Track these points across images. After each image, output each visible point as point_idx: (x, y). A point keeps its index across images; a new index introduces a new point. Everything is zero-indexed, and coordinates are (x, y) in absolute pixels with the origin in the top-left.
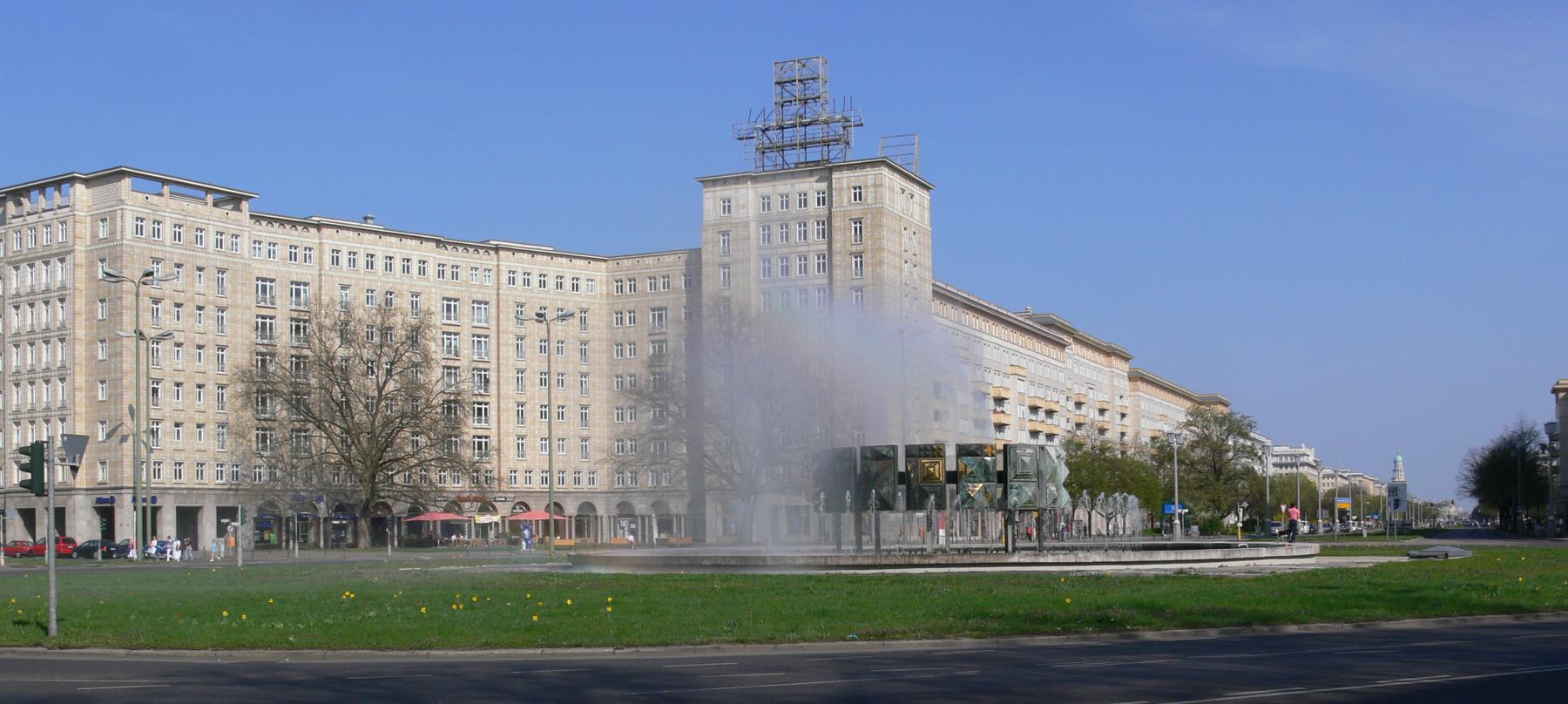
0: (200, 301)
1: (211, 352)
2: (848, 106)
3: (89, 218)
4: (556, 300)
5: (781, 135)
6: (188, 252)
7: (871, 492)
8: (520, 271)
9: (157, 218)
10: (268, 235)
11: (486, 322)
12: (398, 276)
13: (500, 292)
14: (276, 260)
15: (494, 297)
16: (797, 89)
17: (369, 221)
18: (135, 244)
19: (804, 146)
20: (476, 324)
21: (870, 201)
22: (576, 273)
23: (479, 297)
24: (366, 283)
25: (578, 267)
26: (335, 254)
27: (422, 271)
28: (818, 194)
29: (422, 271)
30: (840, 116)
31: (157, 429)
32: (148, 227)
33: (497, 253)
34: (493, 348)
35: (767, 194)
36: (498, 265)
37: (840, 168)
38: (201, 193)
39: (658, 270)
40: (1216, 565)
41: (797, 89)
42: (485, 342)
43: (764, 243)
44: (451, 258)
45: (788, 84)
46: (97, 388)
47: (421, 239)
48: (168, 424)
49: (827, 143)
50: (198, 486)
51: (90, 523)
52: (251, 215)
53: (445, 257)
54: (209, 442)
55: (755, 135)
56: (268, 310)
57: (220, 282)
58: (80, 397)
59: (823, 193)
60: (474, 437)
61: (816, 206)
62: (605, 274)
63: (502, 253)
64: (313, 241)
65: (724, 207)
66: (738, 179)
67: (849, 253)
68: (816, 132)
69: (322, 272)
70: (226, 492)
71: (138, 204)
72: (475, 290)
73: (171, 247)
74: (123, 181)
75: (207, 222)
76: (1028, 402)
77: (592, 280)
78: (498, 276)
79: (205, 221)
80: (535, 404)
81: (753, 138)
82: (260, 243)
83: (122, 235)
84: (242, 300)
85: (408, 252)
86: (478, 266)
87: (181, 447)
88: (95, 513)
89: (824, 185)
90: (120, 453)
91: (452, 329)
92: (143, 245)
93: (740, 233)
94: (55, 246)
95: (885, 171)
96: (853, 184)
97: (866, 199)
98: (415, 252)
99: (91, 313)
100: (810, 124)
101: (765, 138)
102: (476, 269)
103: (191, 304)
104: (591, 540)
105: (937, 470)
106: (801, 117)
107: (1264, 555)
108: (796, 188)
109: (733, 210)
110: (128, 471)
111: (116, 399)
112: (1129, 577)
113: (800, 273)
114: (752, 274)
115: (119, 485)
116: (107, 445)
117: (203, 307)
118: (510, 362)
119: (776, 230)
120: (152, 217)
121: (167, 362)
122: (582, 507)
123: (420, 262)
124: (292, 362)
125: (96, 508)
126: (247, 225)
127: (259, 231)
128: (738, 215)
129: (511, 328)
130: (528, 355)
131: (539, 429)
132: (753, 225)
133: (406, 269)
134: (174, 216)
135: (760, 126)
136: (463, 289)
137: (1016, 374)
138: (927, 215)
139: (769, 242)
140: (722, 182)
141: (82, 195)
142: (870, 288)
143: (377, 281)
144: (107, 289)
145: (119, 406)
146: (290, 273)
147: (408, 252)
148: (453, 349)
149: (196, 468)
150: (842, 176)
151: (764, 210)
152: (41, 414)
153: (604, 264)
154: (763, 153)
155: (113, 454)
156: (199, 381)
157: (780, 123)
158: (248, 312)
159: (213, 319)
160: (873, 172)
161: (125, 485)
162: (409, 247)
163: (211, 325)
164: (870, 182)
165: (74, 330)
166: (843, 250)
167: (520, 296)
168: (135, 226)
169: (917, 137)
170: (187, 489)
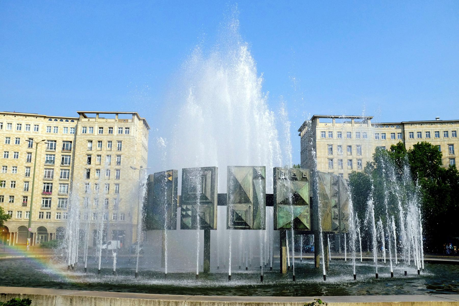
92: (324, 141)
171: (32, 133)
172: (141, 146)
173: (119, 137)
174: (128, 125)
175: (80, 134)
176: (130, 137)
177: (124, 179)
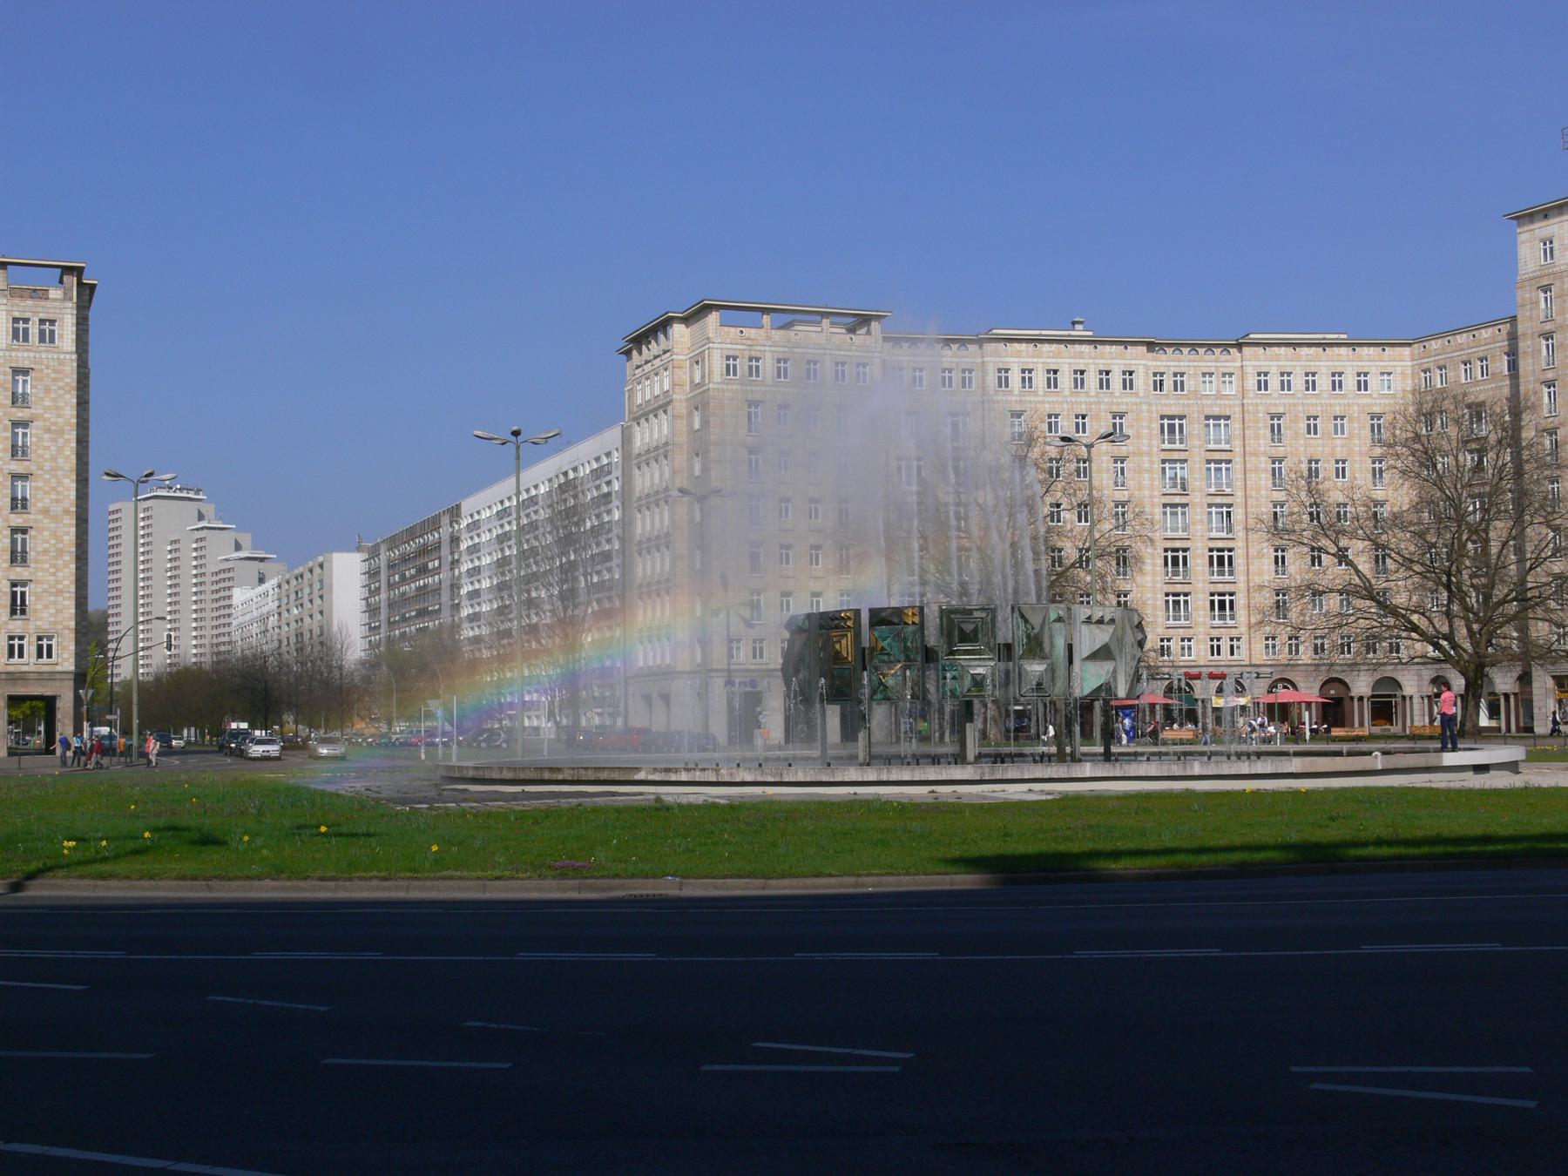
4: (1331, 405)
7: (860, 679)
9: (754, 354)
11: (1228, 442)
12: (1093, 393)
15: (1238, 409)
20: (1212, 446)
22: (1364, 366)
23: (1216, 411)
24: (1047, 406)
25: (1365, 358)
26: (1003, 374)
27: (1128, 385)
29: (1128, 385)
33: (1240, 351)
34: (1239, 476)
38: (819, 318)
39: (1474, 350)
40: (924, 790)
42: (1227, 469)
44: (1173, 363)
47: (1125, 344)
52: (884, 337)
53: (1164, 363)
60: (1167, 595)
62: (1410, 363)
64: (973, 360)
65: (1545, 250)
71: (729, 341)
72: (1209, 402)
75: (822, 352)
77: (1389, 374)
78: (1243, 380)
85: (1105, 361)
86: (1213, 370)
91: (1175, 456)
98: (1115, 361)
102: (1211, 374)
104: (1395, 729)
105: (844, 645)
107: (1088, 775)
109: (1556, 253)
112: (832, 803)
118: (1263, 492)
122: (1379, 683)
133: (1104, 384)
134: (777, 349)
136: (1191, 402)
140: (1556, 211)
141: (682, 336)
143: (1062, 402)
147: (1105, 361)
148: (1179, 481)
167: (1275, 405)
168: (724, 366)
171: (1275, 399)
172: (67, 384)
173: (19, 355)
174: (51, 311)
175: (719, 380)
176: (62, 356)
177: (46, 512)
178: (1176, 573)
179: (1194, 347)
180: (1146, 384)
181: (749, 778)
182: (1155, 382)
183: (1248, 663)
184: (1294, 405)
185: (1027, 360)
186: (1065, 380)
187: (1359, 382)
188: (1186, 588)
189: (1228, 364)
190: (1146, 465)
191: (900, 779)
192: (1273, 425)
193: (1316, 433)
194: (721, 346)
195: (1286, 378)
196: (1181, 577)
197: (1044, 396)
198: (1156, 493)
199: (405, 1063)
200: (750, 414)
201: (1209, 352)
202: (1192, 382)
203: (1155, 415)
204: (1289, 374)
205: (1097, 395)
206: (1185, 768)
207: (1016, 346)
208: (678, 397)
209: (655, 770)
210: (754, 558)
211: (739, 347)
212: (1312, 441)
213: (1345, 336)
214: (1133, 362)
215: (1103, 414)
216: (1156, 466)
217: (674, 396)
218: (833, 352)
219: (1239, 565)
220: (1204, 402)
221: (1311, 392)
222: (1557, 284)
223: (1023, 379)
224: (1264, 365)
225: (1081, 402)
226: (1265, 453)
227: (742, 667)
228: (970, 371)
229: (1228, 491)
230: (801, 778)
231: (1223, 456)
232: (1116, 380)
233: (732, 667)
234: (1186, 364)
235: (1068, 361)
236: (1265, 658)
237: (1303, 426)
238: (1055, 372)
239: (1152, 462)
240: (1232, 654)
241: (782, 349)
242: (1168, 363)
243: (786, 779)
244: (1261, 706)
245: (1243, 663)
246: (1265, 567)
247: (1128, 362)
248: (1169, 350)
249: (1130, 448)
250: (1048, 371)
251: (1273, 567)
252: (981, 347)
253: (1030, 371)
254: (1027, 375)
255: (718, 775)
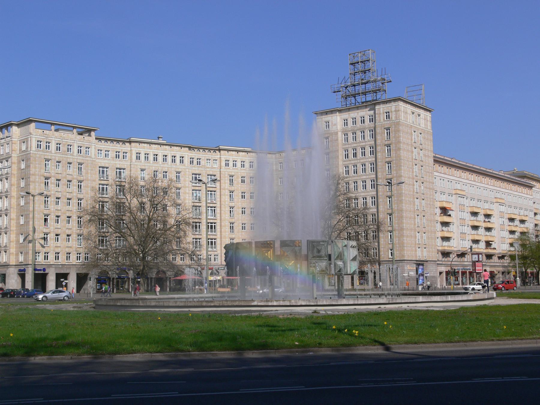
0: (69, 178)
1: (75, 201)
2: (384, 73)
3: (19, 142)
5: (354, 89)
6: (63, 156)
8: (231, 160)
9: (48, 141)
10: (105, 147)
13: (221, 170)
14: (109, 158)
15: (219, 173)
16: (360, 67)
17: (160, 139)
18: (37, 153)
19: (365, 93)
21: (393, 119)
23: (211, 173)
24: (153, 168)
27: (182, 161)
28: (370, 117)
29: (182, 161)
30: (380, 78)
31: (47, 237)
32: (43, 145)
33: (220, 152)
35: (346, 118)
36: (220, 158)
37: (379, 103)
38: (72, 129)
41: (360, 67)
42: (214, 194)
43: (345, 142)
44: (197, 155)
45: (356, 64)
46: (20, 219)
47: (181, 147)
48: (52, 235)
49: (375, 92)
50: (67, 264)
51: (16, 281)
52: (96, 138)
53: (194, 155)
54: (74, 243)
55: (341, 90)
56: (105, 181)
57: (80, 169)
58: (13, 223)
59: (372, 116)
60: (193, 239)
61: (369, 123)
63: (222, 152)
64: (127, 149)
65: (326, 125)
66: (332, 112)
67: (384, 145)
68: (370, 87)
69: (132, 163)
70: (82, 266)
71: (38, 135)
72: (209, 170)
73: (55, 153)
74: (31, 124)
76: (507, 216)
78: (220, 163)
79: (73, 141)
80: (240, 223)
81: (340, 91)
82: (101, 151)
83: (30, 149)
84: (91, 177)
85: (174, 152)
86: (210, 158)
87: (59, 245)
88: (19, 276)
89: (372, 112)
90: (28, 249)
91: (197, 188)
92: (40, 153)
93: (334, 138)
94: (5, 155)
95: (401, 104)
96: (385, 111)
97: (392, 118)
98: (178, 153)
99: (19, 184)
100: (367, 83)
101: (347, 91)
102: (210, 160)
103: (65, 179)
106: (362, 80)
107: (421, 301)
108: (359, 114)
109: (330, 126)
110: (30, 257)
111: (27, 223)
113: (362, 156)
114: (340, 158)
115: (27, 263)
116: (23, 245)
117: (71, 181)
118: (227, 203)
119: (350, 136)
120: (45, 140)
121: (52, 206)
123: (180, 157)
124: (99, 204)
125: (19, 274)
126: (94, 142)
127: (100, 145)
128: (332, 129)
129: (227, 187)
130: (235, 200)
131: (241, 235)
132: (340, 134)
133: (174, 161)
134: (57, 139)
135: (343, 85)
136: (203, 169)
137: (498, 202)
138: (429, 124)
139: (347, 141)
141: (16, 131)
142: (395, 162)
143: (159, 167)
144: (24, 173)
145: (28, 227)
146: (116, 164)
147: (174, 152)
149: (55, 255)
150: (380, 107)
151: (345, 126)
152: (4, 230)
153: (274, 155)
154: (346, 98)
155: (25, 249)
156: (68, 215)
157: (353, 83)
158: (94, 182)
159: (76, 186)
160: (395, 104)
161: (29, 263)
162: (175, 151)
163: (75, 189)
164: (393, 109)
165: (11, 192)
166: (381, 144)
167: (231, 172)
168: (37, 145)
169: (423, 86)
170: (61, 265)
171: (231, 170)
175: (76, 155)
178: (196, 231)
179: (204, 149)
180: (188, 162)
181: (303, 304)
182: (191, 161)
183: (220, 264)
184: (237, 172)
185: (147, 150)
186: (160, 158)
187: (226, 163)
188: (200, 237)
189: (215, 156)
190: (187, 191)
191: (362, 303)
192: (177, 176)
193: (244, 183)
194: (36, 136)
195: (235, 163)
196: (198, 233)
197: (153, 164)
198: (190, 202)
199: (456, 382)
200: (46, 164)
201: (123, 144)
202: (203, 162)
203: (190, 173)
204: (236, 161)
205: (171, 165)
206: (446, 298)
207: (143, 144)
208: (14, 155)
209: (262, 301)
210: (46, 220)
211: (42, 137)
212: (243, 185)
213: (166, 142)
214: (184, 153)
215: (173, 172)
216: (190, 192)
217: (12, 155)
218: (77, 142)
219: (218, 229)
220: (207, 169)
221: (243, 168)
222: (331, 137)
223: (145, 157)
224: (228, 158)
225: (165, 167)
226: (54, 177)
227: (40, 263)
228: (126, 153)
229: (215, 202)
230: (325, 303)
231: (213, 189)
232: (178, 160)
233: (36, 263)
234: (201, 155)
235: (161, 151)
236: (66, 261)
237: (240, 180)
238: (157, 155)
239: (189, 190)
240: (215, 261)
241: (59, 140)
242: (195, 155)
243: (319, 304)
244: (225, 280)
245: (219, 264)
246: (227, 230)
247: (182, 153)
248: (196, 150)
249: (182, 185)
250: (154, 155)
251: (229, 230)
252: (130, 144)
253: (148, 154)
254: (146, 156)
255: (290, 302)
